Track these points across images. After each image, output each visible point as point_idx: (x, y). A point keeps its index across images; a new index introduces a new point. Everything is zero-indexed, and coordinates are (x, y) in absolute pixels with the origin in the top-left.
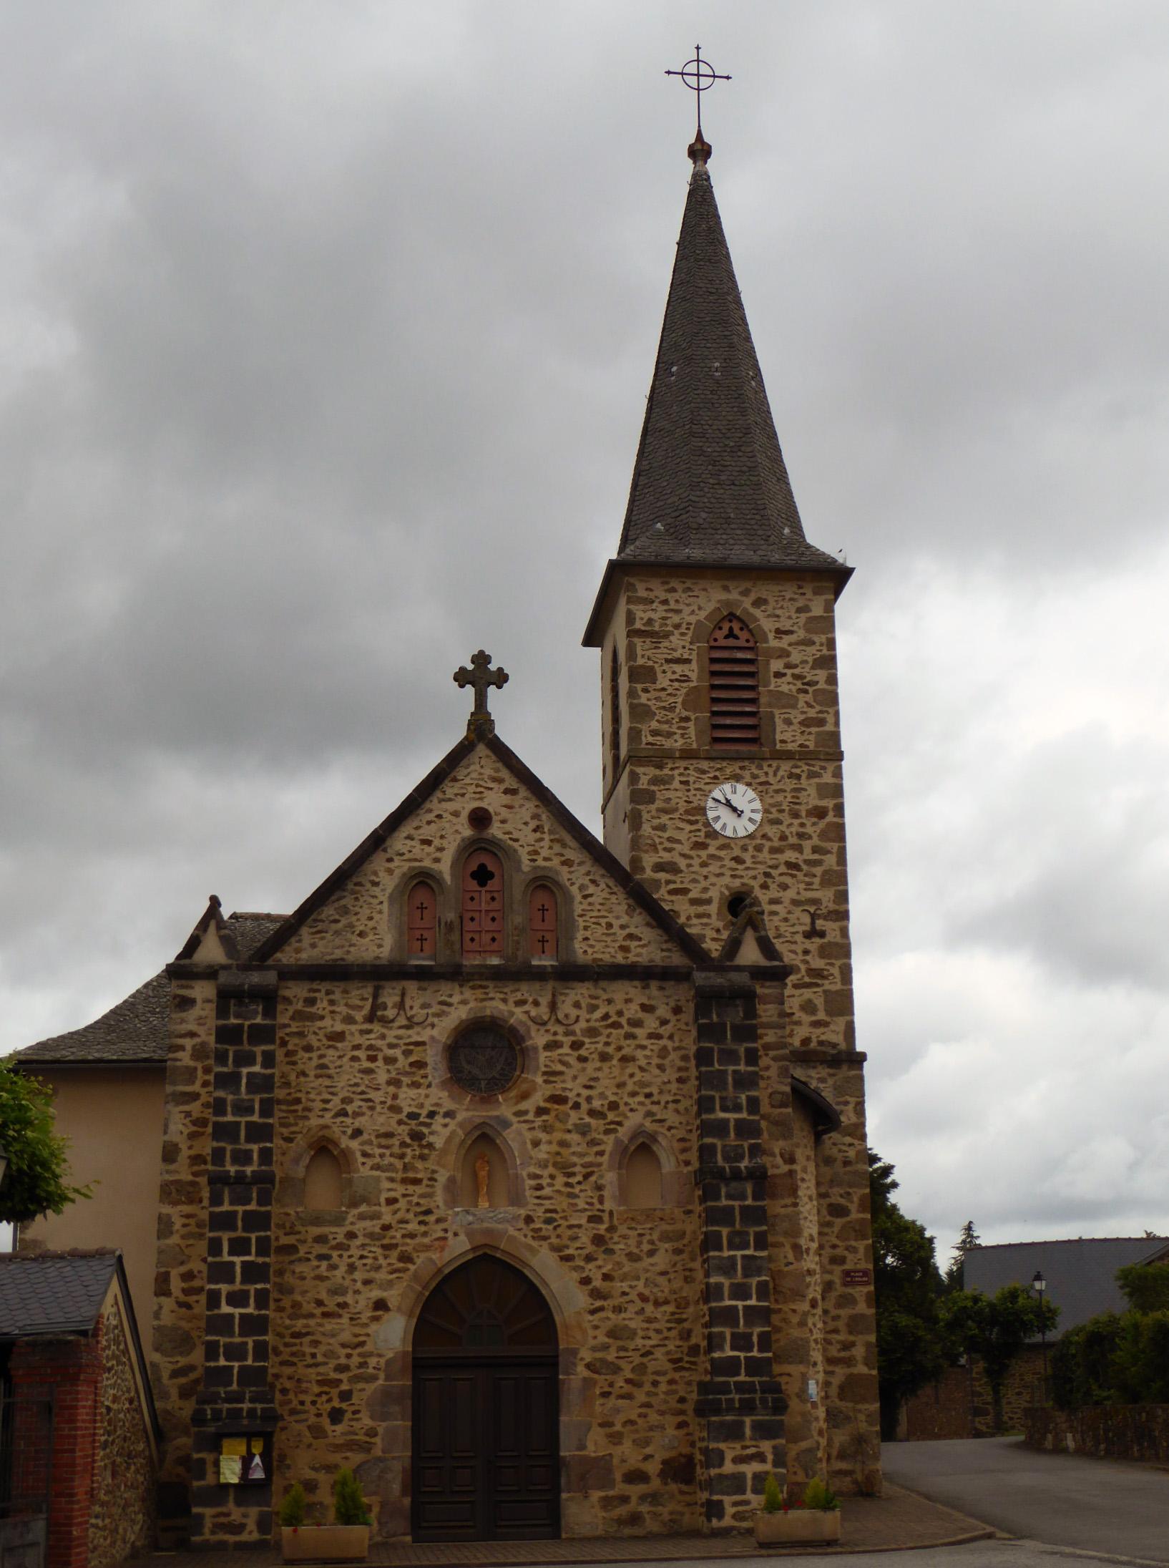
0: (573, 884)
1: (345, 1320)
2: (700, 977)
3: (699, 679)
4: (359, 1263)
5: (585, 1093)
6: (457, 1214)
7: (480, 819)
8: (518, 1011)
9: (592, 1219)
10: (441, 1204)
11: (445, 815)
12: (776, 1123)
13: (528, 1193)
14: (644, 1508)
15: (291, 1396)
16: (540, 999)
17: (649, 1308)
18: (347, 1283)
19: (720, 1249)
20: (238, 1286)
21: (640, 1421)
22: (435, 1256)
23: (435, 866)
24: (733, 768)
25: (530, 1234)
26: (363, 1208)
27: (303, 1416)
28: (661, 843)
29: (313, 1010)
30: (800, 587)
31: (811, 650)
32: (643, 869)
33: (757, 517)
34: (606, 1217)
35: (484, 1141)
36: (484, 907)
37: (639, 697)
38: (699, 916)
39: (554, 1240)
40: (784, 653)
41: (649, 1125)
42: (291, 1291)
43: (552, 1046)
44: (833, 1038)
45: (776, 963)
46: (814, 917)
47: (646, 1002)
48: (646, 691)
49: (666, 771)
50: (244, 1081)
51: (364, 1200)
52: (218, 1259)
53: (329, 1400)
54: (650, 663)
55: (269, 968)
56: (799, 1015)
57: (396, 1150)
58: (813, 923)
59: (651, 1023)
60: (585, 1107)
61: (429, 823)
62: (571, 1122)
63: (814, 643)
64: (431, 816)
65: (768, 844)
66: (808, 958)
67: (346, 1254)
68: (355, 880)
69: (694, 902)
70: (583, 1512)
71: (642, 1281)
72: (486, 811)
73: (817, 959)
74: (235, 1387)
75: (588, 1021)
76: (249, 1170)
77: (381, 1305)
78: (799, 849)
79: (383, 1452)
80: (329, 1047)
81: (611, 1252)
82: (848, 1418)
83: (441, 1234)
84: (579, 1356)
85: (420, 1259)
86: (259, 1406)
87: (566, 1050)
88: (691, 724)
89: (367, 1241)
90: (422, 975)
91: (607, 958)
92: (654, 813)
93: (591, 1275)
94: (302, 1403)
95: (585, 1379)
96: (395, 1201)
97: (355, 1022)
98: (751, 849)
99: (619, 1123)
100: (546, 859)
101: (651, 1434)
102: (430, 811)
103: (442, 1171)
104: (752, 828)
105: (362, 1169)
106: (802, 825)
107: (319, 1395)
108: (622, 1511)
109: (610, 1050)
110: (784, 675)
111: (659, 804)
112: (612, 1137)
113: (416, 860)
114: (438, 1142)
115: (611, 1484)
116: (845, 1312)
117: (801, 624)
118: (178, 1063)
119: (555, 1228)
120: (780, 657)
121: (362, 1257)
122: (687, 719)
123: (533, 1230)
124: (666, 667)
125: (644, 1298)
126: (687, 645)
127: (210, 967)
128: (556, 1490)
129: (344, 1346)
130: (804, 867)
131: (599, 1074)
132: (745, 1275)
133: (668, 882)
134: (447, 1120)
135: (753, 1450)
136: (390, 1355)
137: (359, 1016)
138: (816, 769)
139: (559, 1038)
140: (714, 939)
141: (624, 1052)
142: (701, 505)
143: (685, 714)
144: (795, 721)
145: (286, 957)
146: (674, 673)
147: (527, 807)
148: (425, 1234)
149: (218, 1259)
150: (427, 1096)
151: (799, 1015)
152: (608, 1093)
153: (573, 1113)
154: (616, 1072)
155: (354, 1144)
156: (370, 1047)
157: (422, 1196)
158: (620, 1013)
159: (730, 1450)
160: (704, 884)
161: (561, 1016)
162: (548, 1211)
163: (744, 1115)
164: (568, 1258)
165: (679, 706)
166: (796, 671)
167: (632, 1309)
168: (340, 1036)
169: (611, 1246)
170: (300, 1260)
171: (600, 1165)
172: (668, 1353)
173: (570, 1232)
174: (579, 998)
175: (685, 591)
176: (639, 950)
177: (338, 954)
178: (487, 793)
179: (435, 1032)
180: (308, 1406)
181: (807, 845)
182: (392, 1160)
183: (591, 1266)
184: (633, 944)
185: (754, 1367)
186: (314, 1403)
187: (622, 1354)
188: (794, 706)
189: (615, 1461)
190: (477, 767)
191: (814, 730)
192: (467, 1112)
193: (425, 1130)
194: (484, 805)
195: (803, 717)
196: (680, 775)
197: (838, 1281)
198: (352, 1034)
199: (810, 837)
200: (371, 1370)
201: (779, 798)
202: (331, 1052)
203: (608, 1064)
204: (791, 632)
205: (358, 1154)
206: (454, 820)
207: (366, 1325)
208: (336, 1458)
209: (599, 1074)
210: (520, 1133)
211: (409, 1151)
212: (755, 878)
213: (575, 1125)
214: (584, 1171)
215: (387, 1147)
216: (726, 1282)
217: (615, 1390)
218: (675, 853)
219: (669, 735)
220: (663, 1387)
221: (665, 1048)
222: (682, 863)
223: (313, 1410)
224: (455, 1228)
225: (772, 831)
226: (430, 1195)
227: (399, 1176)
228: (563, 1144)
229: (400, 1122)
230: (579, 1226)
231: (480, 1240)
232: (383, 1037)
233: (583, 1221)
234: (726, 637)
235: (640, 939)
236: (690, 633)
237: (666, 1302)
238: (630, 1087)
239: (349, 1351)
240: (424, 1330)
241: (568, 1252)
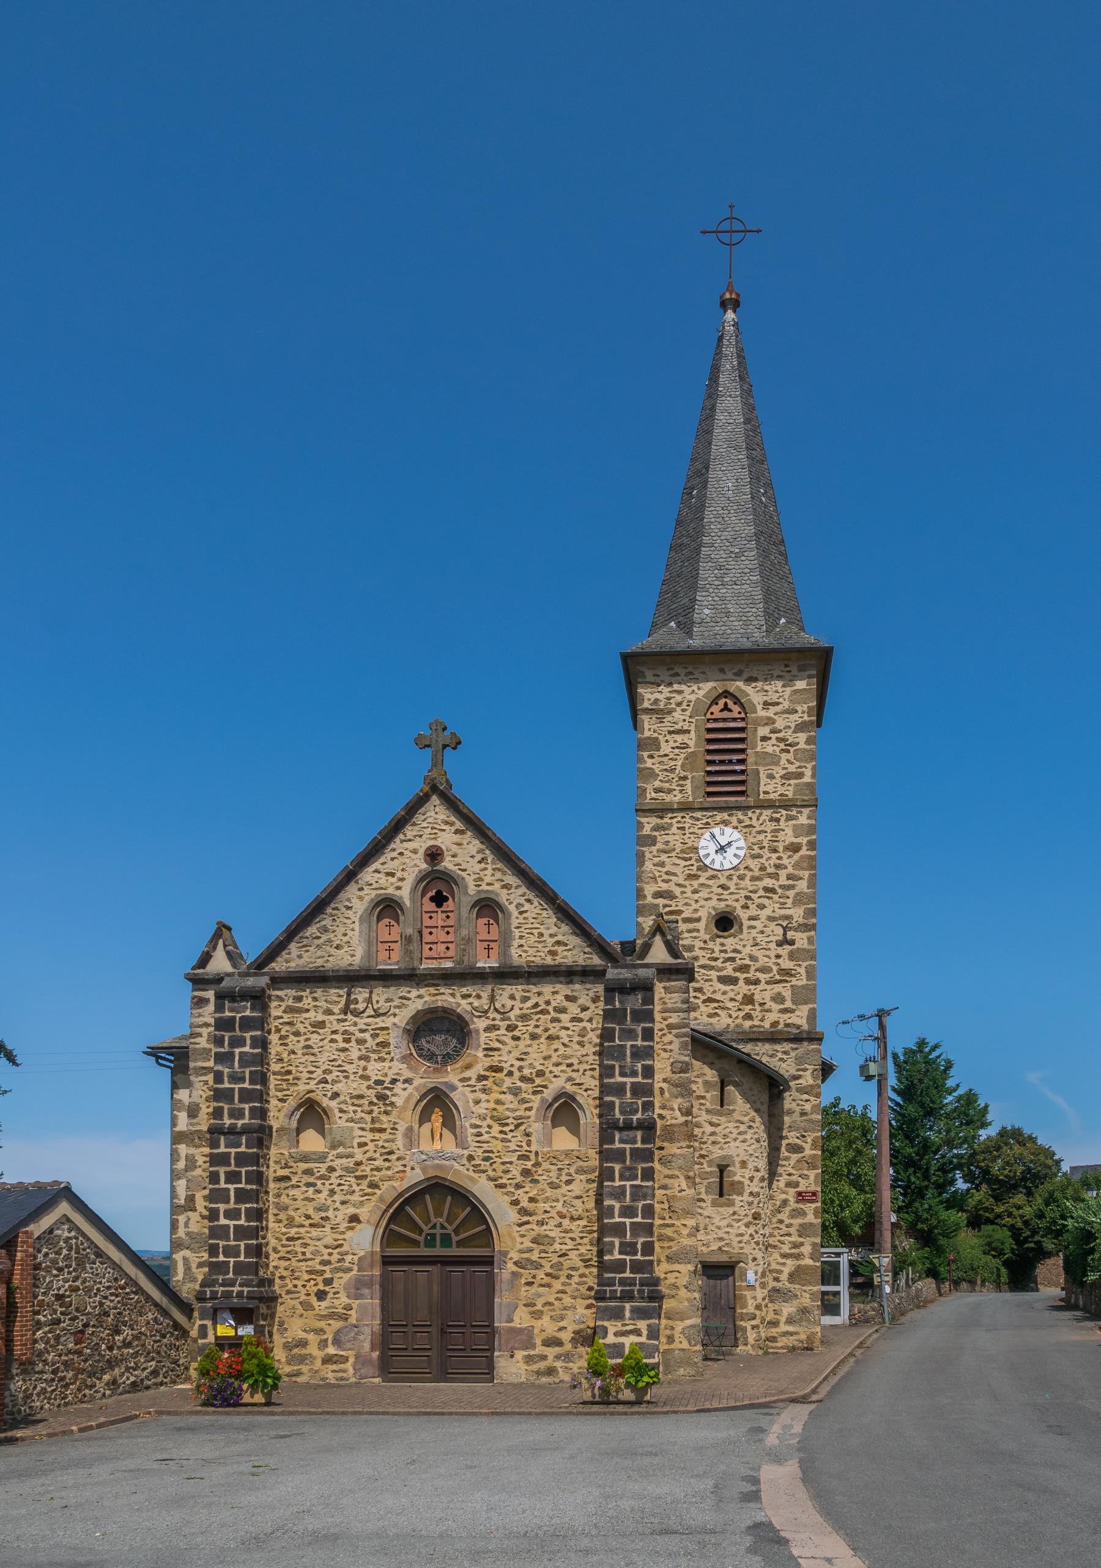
0: (511, 903)
1: (327, 1229)
2: (612, 973)
3: (696, 745)
4: (337, 1189)
5: (518, 1064)
6: (414, 1153)
7: (434, 855)
8: (463, 1002)
9: (520, 1158)
10: (401, 1147)
11: (406, 852)
12: (676, 1086)
13: (469, 1139)
14: (558, 1364)
15: (287, 1281)
16: (482, 994)
17: (566, 1222)
18: (329, 1202)
19: (613, 1180)
20: (232, 1205)
21: (556, 1303)
22: (396, 1184)
23: (398, 893)
24: (721, 816)
26: (341, 1150)
27: (296, 1295)
28: (660, 876)
29: (300, 1005)
30: (786, 666)
31: (795, 717)
32: (645, 897)
33: (754, 610)
34: (532, 1156)
35: (437, 1102)
36: (440, 923)
37: (645, 762)
38: (689, 931)
39: (491, 1173)
40: (770, 721)
41: (569, 1088)
42: (286, 1208)
43: (489, 1029)
44: (798, 1021)
45: (679, 961)
46: (785, 929)
47: (570, 993)
48: (651, 757)
49: (666, 820)
50: (237, 1058)
51: (341, 1144)
52: (216, 1186)
53: (315, 1285)
54: (656, 735)
55: (264, 974)
56: (770, 1004)
57: (367, 1108)
58: (785, 934)
59: (574, 1009)
60: (517, 1074)
61: (392, 859)
62: (505, 1086)
63: (797, 712)
64: (394, 854)
65: (749, 874)
66: (779, 961)
67: (327, 1183)
68: (333, 905)
69: (687, 920)
70: (512, 1367)
71: (561, 1203)
72: (439, 848)
73: (787, 961)
74: (231, 1275)
75: (521, 1009)
76: (240, 1123)
77: (354, 1219)
78: (775, 876)
80: (313, 1032)
81: (536, 1181)
82: (796, 1296)
83: (402, 1168)
86: (246, 1289)
87: (503, 1031)
88: (688, 782)
89: (344, 1173)
90: (387, 978)
91: (538, 960)
92: (655, 853)
94: (295, 1286)
95: (513, 1273)
96: (366, 1144)
97: (334, 1014)
98: (735, 878)
99: (545, 1087)
100: (488, 884)
101: (564, 1312)
102: (394, 850)
103: (402, 1123)
104: (736, 862)
105: (339, 1121)
106: (779, 858)
107: (309, 1281)
108: (542, 1365)
109: (539, 1031)
110: (770, 738)
111: (659, 846)
112: (539, 1096)
113: (382, 888)
114: (399, 1101)
115: (533, 1346)
116: (797, 1222)
117: (786, 697)
118: (197, 1046)
119: (491, 1164)
120: (766, 724)
121: (339, 1185)
122: (685, 778)
124: (668, 737)
125: (562, 1216)
126: (687, 718)
127: (219, 974)
128: (492, 1349)
129: (326, 1247)
130: (779, 891)
131: (529, 1050)
132: (633, 1200)
133: (665, 906)
134: (406, 1085)
135: (631, 1327)
136: (362, 1253)
137: (336, 1009)
138: (794, 813)
139: (497, 1022)
140: (701, 948)
141: (550, 1032)
142: (706, 603)
143: (683, 774)
144: (777, 776)
145: (279, 966)
146: (675, 741)
147: (473, 845)
148: (388, 1168)
149: (216, 1186)
150: (390, 1068)
151: (770, 1004)
152: (536, 1064)
153: (507, 1079)
154: (543, 1047)
155: (333, 1104)
156: (345, 1032)
157: (387, 1141)
158: (548, 1003)
159: (612, 1326)
160: (695, 906)
161: (498, 1005)
162: (485, 1152)
163: (639, 1079)
164: (502, 1186)
165: (679, 768)
166: (780, 735)
167: (552, 1223)
168: (321, 1025)
169: (536, 1177)
170: (293, 1186)
171: (529, 1117)
172: (580, 1255)
173: (503, 1167)
174: (514, 991)
175: (686, 675)
176: (566, 953)
177: (320, 962)
178: (440, 834)
179: (396, 1020)
180: (300, 1288)
181: (783, 874)
182: (363, 1115)
183: (520, 1191)
184: (560, 949)
185: (637, 1267)
186: (304, 1286)
187: (543, 1255)
188: (777, 764)
189: (536, 1331)
190: (433, 814)
191: (792, 782)
192: (423, 1079)
193: (388, 1093)
194: (437, 843)
195: (784, 772)
196: (679, 822)
197: (792, 1200)
198: (331, 1023)
199: (786, 868)
200: (347, 1264)
201: (761, 837)
202: (315, 1036)
203: (537, 1042)
204: (778, 704)
205: (336, 1111)
206: (413, 856)
207: (343, 1233)
208: (322, 1324)
209: (529, 1050)
210: (464, 1095)
211: (375, 1108)
212: (737, 900)
213: (509, 1088)
214: (515, 1122)
215: (359, 1106)
216: (617, 1206)
217: (537, 1281)
218: (672, 884)
219: (670, 791)
220: (576, 1279)
221: (585, 1028)
222: (677, 891)
223: (304, 1291)
224: (412, 1163)
225: (754, 864)
226: (393, 1141)
227: (369, 1126)
228: (498, 1102)
229: (369, 1087)
230: (511, 1163)
232: (355, 1024)
233: (514, 1159)
234: (722, 711)
235: (566, 945)
236: (690, 709)
237: (580, 1218)
238: (554, 1059)
239: (330, 1250)
240: (390, 1237)
241: (500, 1181)
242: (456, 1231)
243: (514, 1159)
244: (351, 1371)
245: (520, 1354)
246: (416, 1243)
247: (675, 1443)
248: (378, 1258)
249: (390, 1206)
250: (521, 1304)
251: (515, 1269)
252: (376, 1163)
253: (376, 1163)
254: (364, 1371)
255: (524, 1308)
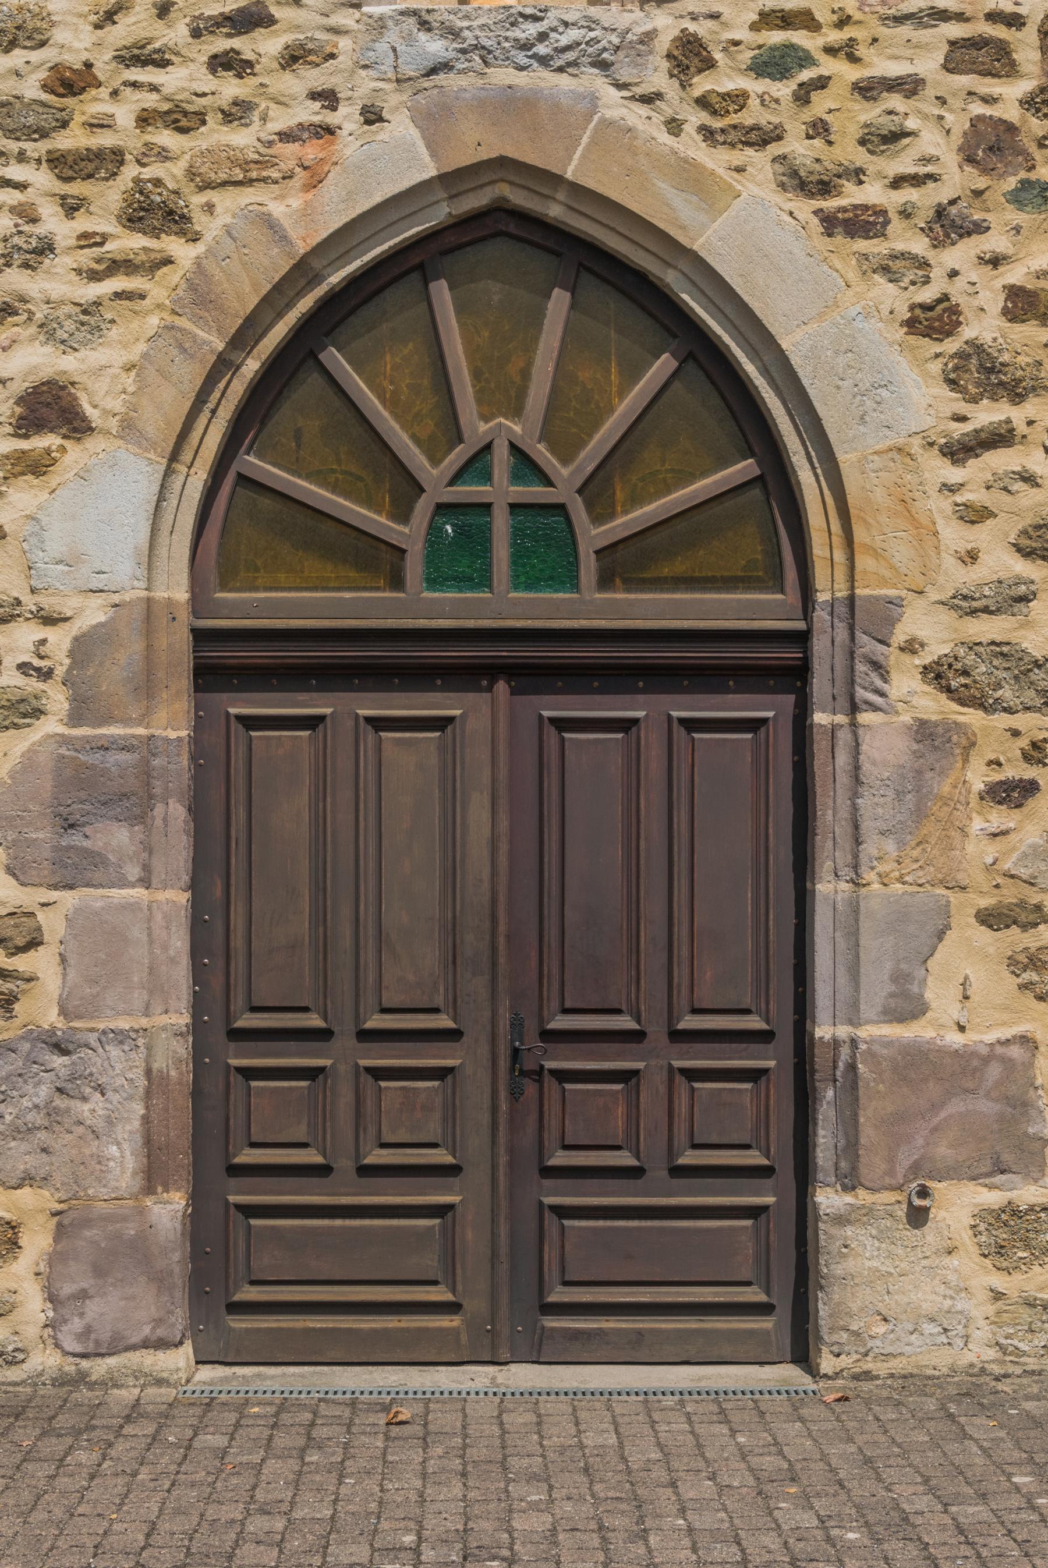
9: (963, 55)
22: (283, 206)
25: (695, 117)
39: (799, 148)
77: (51, 409)
79: (63, 1012)
83: (310, 112)
84: (899, 636)
85: (221, 214)
93: (957, 290)
95: (924, 732)
119: (803, 96)
123: (702, 102)
136: (93, 614)
148: (237, 113)
164: (862, 223)
173: (869, 113)
183: (959, 255)
224: (366, 84)
230: (909, 86)
231: (475, 142)
233: (928, 65)
240: (240, 518)
241: (852, 195)
242: (597, 491)
243: (928, 65)
244: (34, 1307)
245: (959, 1204)
246: (380, 561)
247: (178, 1370)
248: (177, 643)
249: (243, 338)
250: (964, 908)
251: (932, 705)
252: (173, 80)
253: (173, 80)
254: (103, 1310)
255: (983, 935)
